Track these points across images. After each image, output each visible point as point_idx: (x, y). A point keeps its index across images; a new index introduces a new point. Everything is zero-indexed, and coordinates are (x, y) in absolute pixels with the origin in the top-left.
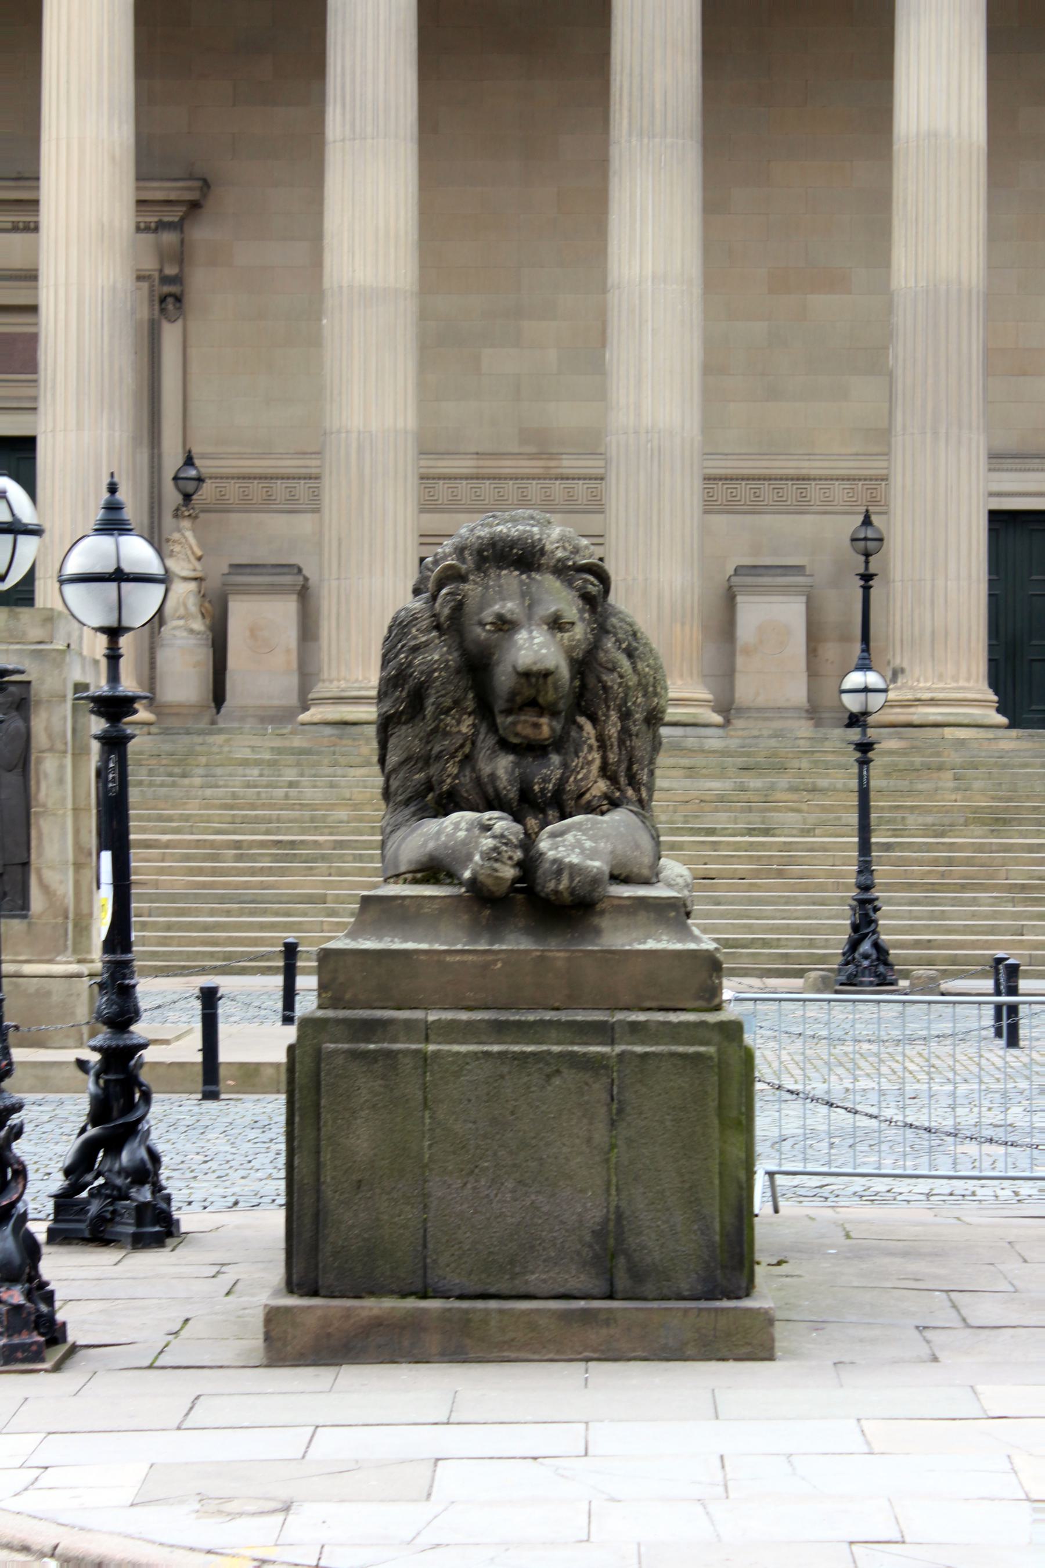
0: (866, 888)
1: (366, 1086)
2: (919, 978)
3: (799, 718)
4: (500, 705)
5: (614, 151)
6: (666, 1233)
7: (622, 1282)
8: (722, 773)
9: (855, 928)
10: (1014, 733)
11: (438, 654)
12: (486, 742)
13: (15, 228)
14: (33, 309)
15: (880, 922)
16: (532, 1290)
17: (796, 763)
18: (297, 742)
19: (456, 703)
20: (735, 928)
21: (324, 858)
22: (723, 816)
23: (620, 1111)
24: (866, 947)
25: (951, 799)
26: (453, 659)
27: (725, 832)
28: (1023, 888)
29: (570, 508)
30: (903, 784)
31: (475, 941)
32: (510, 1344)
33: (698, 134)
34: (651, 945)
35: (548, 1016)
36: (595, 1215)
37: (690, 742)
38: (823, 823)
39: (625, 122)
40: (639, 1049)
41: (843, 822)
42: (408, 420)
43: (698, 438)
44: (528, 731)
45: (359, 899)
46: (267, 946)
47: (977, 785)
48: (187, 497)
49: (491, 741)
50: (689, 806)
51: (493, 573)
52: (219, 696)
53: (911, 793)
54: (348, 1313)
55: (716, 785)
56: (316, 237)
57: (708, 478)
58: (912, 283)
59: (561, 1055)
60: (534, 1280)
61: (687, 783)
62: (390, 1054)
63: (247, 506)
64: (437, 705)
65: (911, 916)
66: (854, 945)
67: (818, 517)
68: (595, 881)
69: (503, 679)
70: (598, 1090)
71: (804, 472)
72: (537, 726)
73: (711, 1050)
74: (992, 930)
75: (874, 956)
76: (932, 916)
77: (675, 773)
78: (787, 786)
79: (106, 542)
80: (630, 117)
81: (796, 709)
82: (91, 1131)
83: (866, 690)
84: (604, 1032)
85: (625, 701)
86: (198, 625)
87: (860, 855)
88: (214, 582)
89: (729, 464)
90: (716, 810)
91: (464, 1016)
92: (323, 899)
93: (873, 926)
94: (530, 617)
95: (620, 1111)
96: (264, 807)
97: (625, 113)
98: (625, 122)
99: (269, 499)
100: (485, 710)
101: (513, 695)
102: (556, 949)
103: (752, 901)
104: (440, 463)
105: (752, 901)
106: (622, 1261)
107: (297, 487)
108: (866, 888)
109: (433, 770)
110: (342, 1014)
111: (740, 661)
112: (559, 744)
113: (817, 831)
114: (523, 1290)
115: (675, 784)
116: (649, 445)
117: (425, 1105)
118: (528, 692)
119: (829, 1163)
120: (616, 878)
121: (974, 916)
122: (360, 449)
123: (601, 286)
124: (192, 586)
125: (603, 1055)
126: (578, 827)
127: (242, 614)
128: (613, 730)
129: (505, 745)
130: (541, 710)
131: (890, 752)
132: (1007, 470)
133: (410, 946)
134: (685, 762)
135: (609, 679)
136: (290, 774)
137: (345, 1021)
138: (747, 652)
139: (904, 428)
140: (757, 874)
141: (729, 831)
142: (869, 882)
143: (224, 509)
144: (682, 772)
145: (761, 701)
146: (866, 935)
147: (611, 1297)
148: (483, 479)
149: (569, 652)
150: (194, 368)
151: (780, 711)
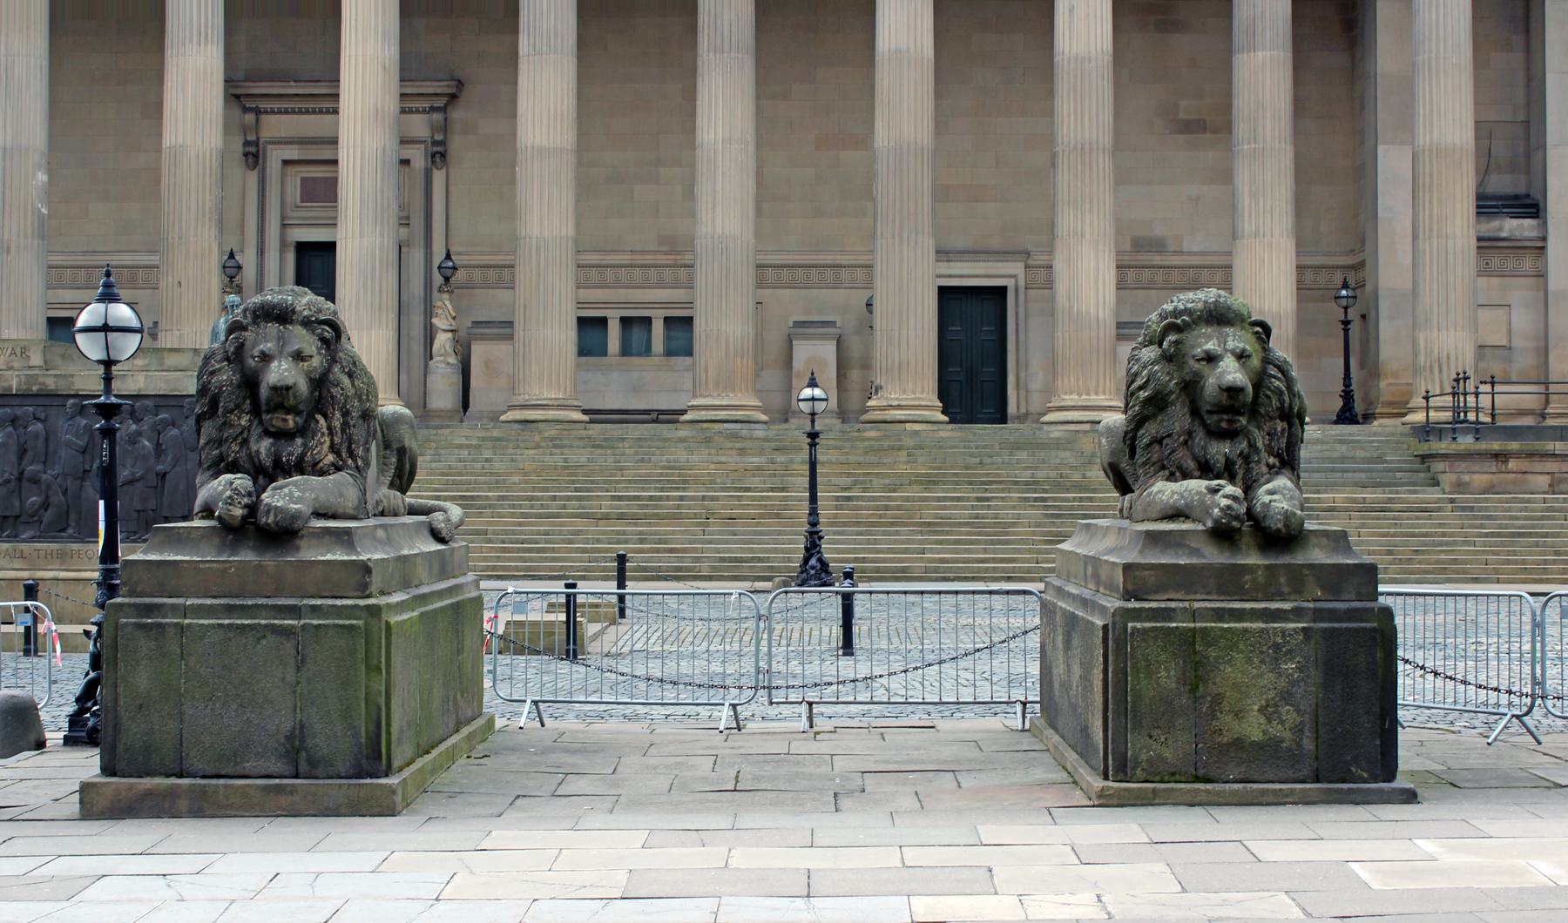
0: (814, 524)
1: (145, 645)
4: (264, 408)
6: (333, 737)
7: (303, 767)
8: (761, 452)
9: (807, 549)
10: (950, 426)
11: (226, 376)
12: (256, 430)
13: (328, 112)
14: (335, 162)
16: (247, 772)
18: (496, 433)
19: (237, 406)
21: (490, 506)
22: (757, 479)
23: (303, 661)
24: (813, 562)
25: (903, 469)
26: (236, 379)
28: (929, 524)
30: (874, 459)
31: (219, 554)
32: (231, 806)
33: (752, 50)
34: (329, 557)
35: (260, 601)
36: (287, 726)
40: (315, 622)
42: (570, 231)
44: (280, 424)
47: (921, 459)
48: (447, 279)
49: (259, 430)
51: (262, 325)
52: (466, 405)
53: (878, 464)
54: (131, 787)
56: (513, 115)
57: (758, 266)
59: (266, 626)
60: (248, 766)
61: (738, 459)
62: (160, 626)
63: (486, 286)
64: (225, 408)
65: (855, 542)
66: (806, 560)
68: (295, 516)
69: (264, 392)
70: (289, 646)
72: (285, 420)
73: (361, 622)
74: (905, 551)
76: (869, 542)
79: (101, 306)
82: (92, 675)
83: (813, 399)
84: (294, 611)
85: (345, 405)
86: (452, 360)
88: (463, 334)
91: (209, 602)
92: (485, 532)
94: (281, 353)
95: (303, 661)
96: (467, 474)
99: (500, 280)
100: (256, 411)
101: (269, 401)
102: (269, 560)
106: (303, 754)
107: (502, 274)
108: (814, 524)
109: (224, 448)
110: (133, 600)
112: (303, 431)
114: (242, 772)
117: (182, 658)
118: (277, 400)
119: (556, 693)
120: (318, 515)
121: (895, 542)
122: (538, 249)
123: (692, 144)
124: (450, 335)
125: (293, 626)
126: (295, 484)
127: (478, 351)
128: (337, 423)
129: (267, 433)
130: (289, 411)
131: (1317, 442)
133: (179, 558)
135: (334, 391)
136: (487, 454)
137: (134, 605)
140: (762, 516)
143: (469, 285)
147: (296, 776)
149: (308, 374)
150: (453, 199)
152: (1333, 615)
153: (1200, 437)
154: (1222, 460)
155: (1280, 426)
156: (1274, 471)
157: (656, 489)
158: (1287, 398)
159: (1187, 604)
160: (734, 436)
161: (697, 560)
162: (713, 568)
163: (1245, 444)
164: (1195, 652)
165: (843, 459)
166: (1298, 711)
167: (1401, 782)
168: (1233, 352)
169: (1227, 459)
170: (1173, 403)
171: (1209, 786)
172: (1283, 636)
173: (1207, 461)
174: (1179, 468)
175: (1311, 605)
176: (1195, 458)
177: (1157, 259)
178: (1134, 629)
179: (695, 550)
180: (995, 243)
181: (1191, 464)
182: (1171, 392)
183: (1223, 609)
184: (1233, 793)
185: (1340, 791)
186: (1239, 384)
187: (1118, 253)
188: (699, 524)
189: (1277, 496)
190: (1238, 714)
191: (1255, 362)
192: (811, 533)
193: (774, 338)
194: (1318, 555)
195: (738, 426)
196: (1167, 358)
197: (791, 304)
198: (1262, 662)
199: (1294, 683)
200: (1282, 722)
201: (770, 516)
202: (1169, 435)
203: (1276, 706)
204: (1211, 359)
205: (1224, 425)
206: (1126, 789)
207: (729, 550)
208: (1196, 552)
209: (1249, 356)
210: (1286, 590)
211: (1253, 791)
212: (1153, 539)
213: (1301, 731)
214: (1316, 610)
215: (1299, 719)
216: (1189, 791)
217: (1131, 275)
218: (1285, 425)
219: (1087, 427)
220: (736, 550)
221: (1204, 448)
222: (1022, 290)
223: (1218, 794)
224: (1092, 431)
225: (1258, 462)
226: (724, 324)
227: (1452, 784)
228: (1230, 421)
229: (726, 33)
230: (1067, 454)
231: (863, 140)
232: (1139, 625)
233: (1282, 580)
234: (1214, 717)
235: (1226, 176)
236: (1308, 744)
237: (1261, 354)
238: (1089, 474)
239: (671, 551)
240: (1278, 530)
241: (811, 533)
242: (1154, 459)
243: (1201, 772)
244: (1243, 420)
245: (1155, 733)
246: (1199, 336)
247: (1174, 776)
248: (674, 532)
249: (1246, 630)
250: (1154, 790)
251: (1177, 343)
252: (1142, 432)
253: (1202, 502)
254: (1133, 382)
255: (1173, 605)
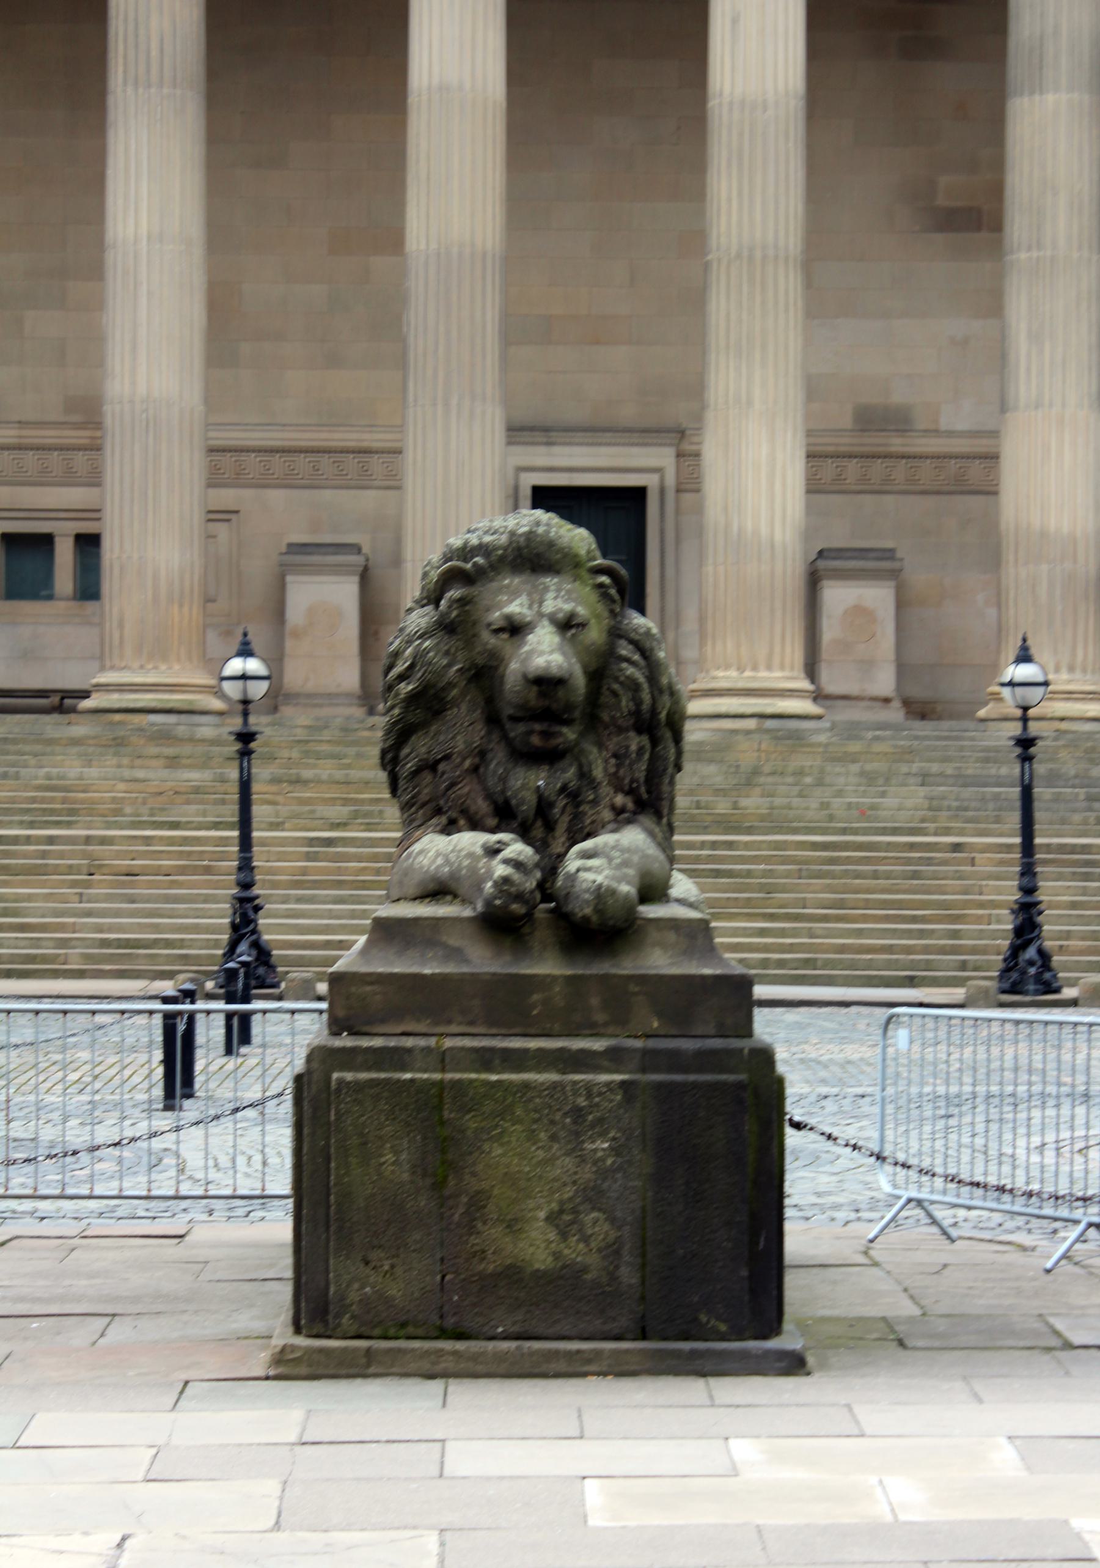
2: (293, 980)
3: (350, 705)
5: (111, 100)
9: (235, 927)
15: (1045, 928)
17: (285, 753)
20: (141, 928)
24: (1031, 953)
27: (189, 826)
29: (69, 479)
37: (181, 731)
38: (297, 816)
39: (121, 69)
41: (318, 815)
43: (201, 408)
45: (229, 898)
46: (804, 952)
50: (160, 799)
55: (195, 776)
57: (212, 450)
58: (423, 247)
61: (165, 773)
65: (331, 915)
66: (1016, 951)
67: (381, 492)
71: (365, 444)
75: (1039, 963)
77: (154, 763)
78: (269, 777)
80: (125, 64)
81: (348, 695)
83: (244, 677)
87: (1024, 857)
89: (286, 435)
90: (188, 802)
93: (251, 927)
97: (121, 60)
98: (121, 69)
103: (168, 899)
104: (336, 436)
105: (168, 899)
108: (246, 885)
111: (289, 644)
113: (287, 825)
115: (151, 775)
116: (144, 416)
132: (578, 444)
134: (170, 751)
138: (296, 635)
139: (415, 401)
140: (183, 870)
141: (193, 825)
142: (248, 879)
144: (162, 762)
145: (310, 687)
146: (244, 935)
148: (26, 449)
151: (332, 698)
152: (674, 1061)
153: (498, 757)
154: (531, 799)
155: (635, 742)
156: (622, 818)
157: (21, 824)
158: (646, 696)
159: (432, 1042)
160: (164, 736)
161: (63, 943)
162: (88, 958)
163: (570, 774)
164: (442, 1123)
165: (339, 775)
166: (612, 1220)
167: (788, 1340)
168: (553, 619)
169: (541, 799)
170: (455, 703)
171: (460, 1346)
172: (589, 1096)
173: (507, 802)
174: (464, 812)
175: (638, 1044)
176: (489, 796)
177: (897, 444)
178: (341, 1082)
179: (61, 928)
180: (628, 413)
181: (481, 806)
182: (451, 685)
183: (492, 1050)
184: (501, 1357)
185: (676, 1354)
186: (554, 671)
187: (809, 433)
188: (74, 884)
189: (603, 862)
190: (514, 1226)
191: (595, 634)
192: (242, 901)
193: (258, 566)
194: (659, 961)
195: (172, 719)
196: (446, 627)
197: (282, 514)
198: (553, 1138)
199: (604, 1174)
200: (586, 1239)
201: (195, 870)
202: (447, 757)
203: (575, 1211)
204: (515, 629)
205: (536, 740)
206: (321, 1350)
207: (120, 929)
208: (454, 954)
209: (583, 625)
210: (600, 1017)
211: (532, 1353)
212: (387, 932)
213: (617, 1253)
214: (645, 1052)
215: (613, 1234)
216: (427, 1353)
217: (829, 469)
218: (645, 740)
219: (751, 724)
220: (129, 926)
221: (503, 779)
222: (670, 496)
223: (475, 1358)
224: (760, 730)
225: (595, 802)
226: (154, 542)
227: (892, 1341)
228: (546, 735)
229: (154, 53)
230: (711, 769)
231: (392, 239)
232: (349, 1076)
233: (595, 1001)
234: (472, 1230)
235: (992, 304)
236: (628, 1276)
237: (606, 622)
238: (744, 802)
239: (22, 928)
240: (586, 919)
241: (242, 901)
242: (423, 797)
243: (450, 1322)
244: (570, 734)
245: (373, 1255)
246: (500, 591)
247: (404, 1328)
248: (30, 898)
249: (526, 1086)
250: (368, 1350)
251: (462, 602)
252: (405, 751)
253: (473, 870)
254: (390, 667)
255: (409, 1042)
